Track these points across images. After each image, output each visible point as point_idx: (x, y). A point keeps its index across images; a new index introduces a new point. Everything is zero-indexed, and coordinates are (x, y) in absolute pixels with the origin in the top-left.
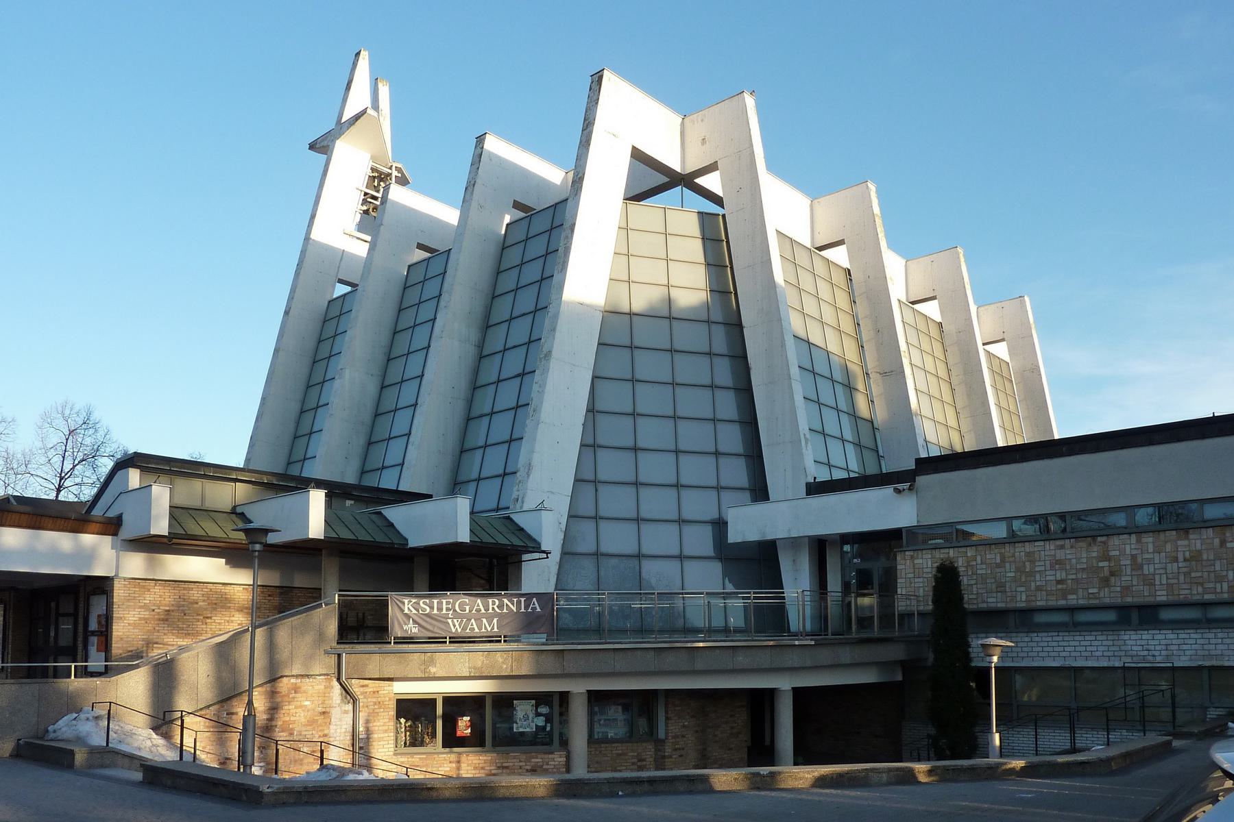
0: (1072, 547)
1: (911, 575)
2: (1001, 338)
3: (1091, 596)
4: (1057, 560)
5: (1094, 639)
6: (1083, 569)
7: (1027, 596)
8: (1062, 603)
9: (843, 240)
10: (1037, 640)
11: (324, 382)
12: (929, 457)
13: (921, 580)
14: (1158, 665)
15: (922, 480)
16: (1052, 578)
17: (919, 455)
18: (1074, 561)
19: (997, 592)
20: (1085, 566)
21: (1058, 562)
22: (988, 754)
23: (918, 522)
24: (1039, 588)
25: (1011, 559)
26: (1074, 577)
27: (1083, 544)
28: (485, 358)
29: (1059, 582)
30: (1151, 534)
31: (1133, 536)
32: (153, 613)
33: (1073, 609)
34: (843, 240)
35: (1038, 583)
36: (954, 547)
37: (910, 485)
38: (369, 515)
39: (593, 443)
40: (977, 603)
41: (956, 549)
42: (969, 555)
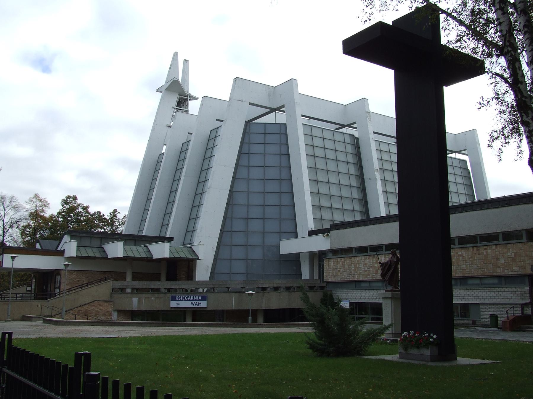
0: (369, 259)
1: (328, 268)
2: (465, 149)
3: (373, 277)
4: (365, 263)
5: (508, 292)
6: (371, 267)
7: (357, 276)
8: (366, 279)
9: (356, 122)
10: (489, 292)
11: (202, 193)
12: (355, 220)
13: (330, 270)
14: (157, 293)
15: (333, 233)
16: (363, 270)
17: (381, 215)
18: (369, 264)
19: (350, 275)
20: (372, 266)
21: (365, 264)
22: (248, 321)
23: (330, 248)
24: (360, 274)
25: (353, 262)
26: (369, 269)
27: (371, 258)
28: (335, 153)
29: (366, 271)
30: (388, 255)
31: (384, 255)
32: (74, 281)
33: (370, 281)
34: (356, 122)
35: (360, 272)
36: (368, 255)
37: (327, 235)
38: (181, 248)
39: (319, 205)
40: (345, 279)
41: (339, 258)
42: (343, 261)
